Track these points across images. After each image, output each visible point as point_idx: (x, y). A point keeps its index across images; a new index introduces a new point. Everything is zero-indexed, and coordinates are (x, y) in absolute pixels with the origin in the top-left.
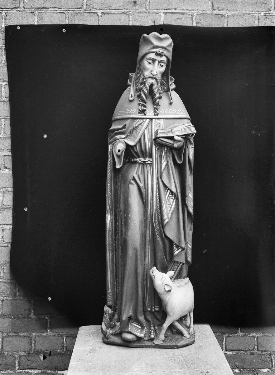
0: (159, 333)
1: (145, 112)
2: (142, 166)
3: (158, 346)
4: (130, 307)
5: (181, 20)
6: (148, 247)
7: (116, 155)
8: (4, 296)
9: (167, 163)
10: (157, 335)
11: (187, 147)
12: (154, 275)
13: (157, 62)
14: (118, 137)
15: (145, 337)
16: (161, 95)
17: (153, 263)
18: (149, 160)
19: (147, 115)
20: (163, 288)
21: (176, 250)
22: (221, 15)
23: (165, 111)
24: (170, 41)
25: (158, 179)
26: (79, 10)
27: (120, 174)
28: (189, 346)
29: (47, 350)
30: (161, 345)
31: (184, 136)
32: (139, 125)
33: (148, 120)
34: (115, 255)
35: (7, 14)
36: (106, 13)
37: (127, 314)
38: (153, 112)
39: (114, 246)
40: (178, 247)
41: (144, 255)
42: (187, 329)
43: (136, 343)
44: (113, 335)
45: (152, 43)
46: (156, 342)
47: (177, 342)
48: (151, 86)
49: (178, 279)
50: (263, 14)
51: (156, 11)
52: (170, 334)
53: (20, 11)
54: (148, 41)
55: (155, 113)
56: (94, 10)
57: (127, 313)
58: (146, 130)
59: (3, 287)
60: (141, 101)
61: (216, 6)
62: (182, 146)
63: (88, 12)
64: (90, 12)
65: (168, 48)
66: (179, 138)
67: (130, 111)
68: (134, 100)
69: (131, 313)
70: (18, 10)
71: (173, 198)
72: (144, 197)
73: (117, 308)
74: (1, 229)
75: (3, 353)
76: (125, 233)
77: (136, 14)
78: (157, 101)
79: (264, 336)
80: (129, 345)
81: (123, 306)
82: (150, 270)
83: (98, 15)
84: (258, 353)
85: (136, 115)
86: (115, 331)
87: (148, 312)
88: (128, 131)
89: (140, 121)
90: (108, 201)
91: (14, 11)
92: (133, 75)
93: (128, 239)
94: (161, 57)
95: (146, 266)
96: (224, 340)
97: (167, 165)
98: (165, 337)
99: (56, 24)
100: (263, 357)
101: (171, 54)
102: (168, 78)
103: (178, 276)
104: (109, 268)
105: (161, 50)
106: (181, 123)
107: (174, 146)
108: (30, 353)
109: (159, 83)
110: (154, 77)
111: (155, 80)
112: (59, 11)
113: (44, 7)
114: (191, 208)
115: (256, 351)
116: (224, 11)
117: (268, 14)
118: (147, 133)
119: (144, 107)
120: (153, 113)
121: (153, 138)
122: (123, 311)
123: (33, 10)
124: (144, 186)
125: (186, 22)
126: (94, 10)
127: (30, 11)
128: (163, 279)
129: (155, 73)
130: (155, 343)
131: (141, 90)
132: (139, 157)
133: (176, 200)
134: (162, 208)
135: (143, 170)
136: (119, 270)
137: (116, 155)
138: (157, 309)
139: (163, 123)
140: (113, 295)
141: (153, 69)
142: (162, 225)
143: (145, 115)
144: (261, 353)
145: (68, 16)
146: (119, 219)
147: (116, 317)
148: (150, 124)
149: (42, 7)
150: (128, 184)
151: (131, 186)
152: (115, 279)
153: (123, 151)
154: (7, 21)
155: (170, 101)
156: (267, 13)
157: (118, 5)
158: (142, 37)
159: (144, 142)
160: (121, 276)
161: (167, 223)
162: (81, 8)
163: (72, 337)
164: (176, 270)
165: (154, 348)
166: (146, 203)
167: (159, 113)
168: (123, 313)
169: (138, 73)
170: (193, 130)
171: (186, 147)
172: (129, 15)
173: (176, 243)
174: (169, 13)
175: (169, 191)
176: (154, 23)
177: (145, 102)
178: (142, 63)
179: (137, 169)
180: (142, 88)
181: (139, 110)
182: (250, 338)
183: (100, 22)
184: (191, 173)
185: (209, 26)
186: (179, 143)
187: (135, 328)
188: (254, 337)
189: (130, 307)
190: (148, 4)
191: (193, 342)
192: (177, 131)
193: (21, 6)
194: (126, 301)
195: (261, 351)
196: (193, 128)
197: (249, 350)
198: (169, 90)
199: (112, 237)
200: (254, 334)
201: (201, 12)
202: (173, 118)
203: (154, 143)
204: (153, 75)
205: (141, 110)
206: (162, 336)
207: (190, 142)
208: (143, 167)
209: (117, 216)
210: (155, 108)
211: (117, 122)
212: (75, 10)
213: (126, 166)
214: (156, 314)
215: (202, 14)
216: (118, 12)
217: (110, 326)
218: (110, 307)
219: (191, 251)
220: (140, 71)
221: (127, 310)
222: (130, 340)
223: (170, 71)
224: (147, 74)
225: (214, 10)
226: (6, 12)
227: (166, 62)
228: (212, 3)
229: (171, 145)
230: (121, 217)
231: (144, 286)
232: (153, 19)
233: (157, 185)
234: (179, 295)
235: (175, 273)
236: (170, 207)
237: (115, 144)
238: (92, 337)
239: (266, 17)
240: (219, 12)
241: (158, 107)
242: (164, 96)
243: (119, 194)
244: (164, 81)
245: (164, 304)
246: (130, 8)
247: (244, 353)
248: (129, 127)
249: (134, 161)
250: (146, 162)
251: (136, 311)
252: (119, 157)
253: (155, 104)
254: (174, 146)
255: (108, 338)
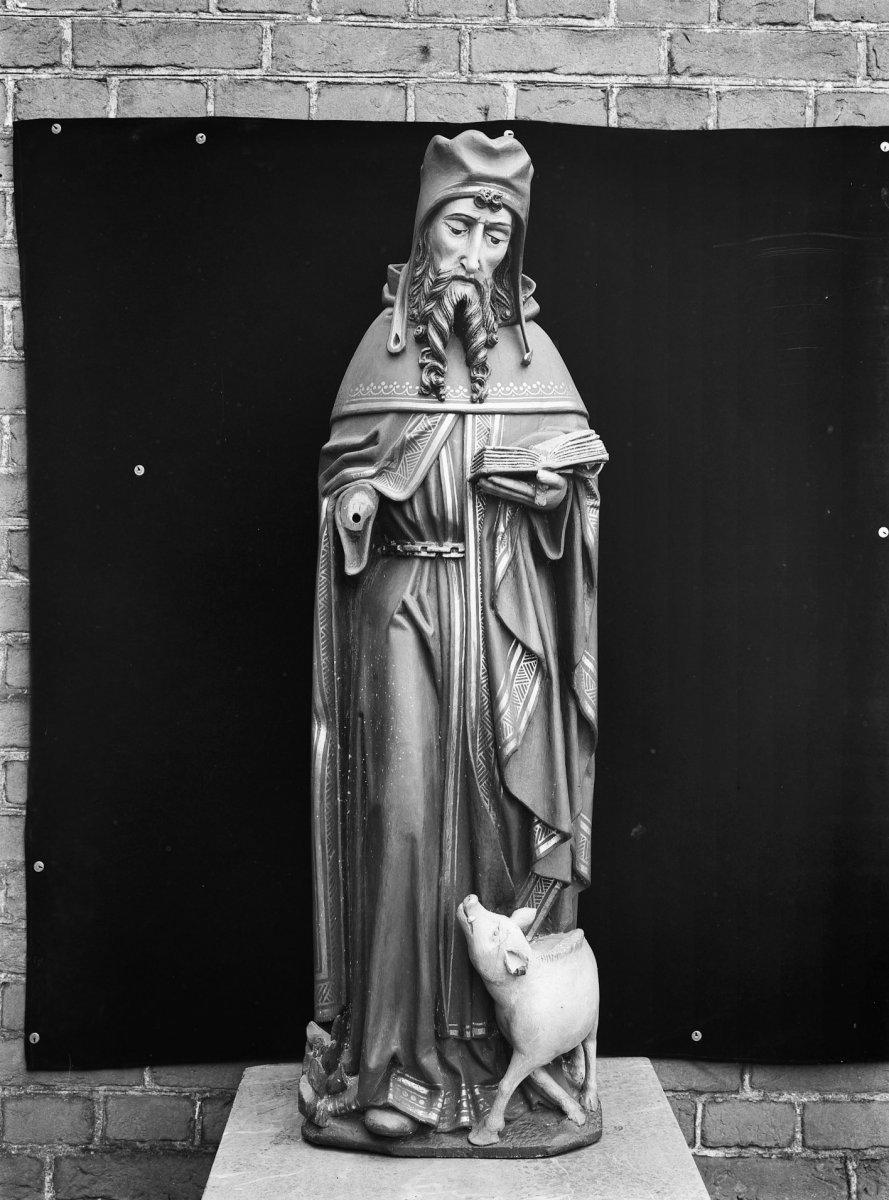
0: (485, 1107)
1: (441, 393)
2: (430, 569)
3: (483, 1150)
4: (391, 1027)
5: (570, 107)
6: (451, 831)
7: (347, 530)
8: (9, 972)
9: (514, 557)
10: (479, 1116)
11: (579, 504)
12: (471, 923)
13: (480, 228)
14: (351, 471)
15: (440, 1121)
16: (495, 337)
17: (467, 884)
18: (455, 549)
19: (449, 402)
20: (500, 965)
21: (543, 839)
22: (699, 89)
23: (506, 389)
24: (524, 158)
25: (484, 611)
26: (247, 72)
27: (359, 596)
28: (585, 1152)
29: (142, 1142)
30: (494, 1146)
31: (570, 471)
32: (423, 433)
33: (451, 417)
34: (344, 858)
35: (21, 86)
36: (334, 83)
37: (383, 1050)
38: (466, 390)
39: (339, 828)
40: (549, 829)
41: (437, 856)
42: (575, 1095)
43: (414, 1143)
44: (336, 1115)
45: (463, 167)
46: (478, 1139)
47: (543, 1138)
48: (462, 305)
49: (548, 933)
50: (831, 90)
51: (491, 77)
52: (521, 1111)
53: (62, 76)
54: (450, 160)
55: (475, 396)
56: (292, 73)
57: (383, 1043)
58: (444, 450)
59: (5, 943)
60: (428, 357)
61: (681, 62)
62: (558, 508)
63: (276, 78)
64: (283, 78)
65: (516, 183)
66: (554, 478)
67: (391, 386)
68: (403, 350)
69: (395, 1046)
70: (56, 71)
71: (533, 673)
72: (438, 669)
73: (351, 1028)
74: (2, 761)
75: (5, 1150)
76: (377, 786)
77: (429, 88)
78: (481, 355)
79: (826, 1101)
80: (390, 1148)
81: (371, 1022)
82: (457, 906)
83: (308, 90)
84: (804, 1155)
85: (412, 401)
86: (342, 1105)
87: (449, 1042)
88: (387, 455)
89: (426, 422)
90: (320, 682)
91: (44, 74)
92: (400, 269)
93: (386, 806)
94: (493, 211)
95: (443, 891)
96: (699, 1115)
97: (514, 563)
98: (507, 1121)
99: (174, 115)
100: (820, 1166)
101: (527, 201)
102: (517, 283)
103: (549, 925)
104: (321, 899)
105: (494, 190)
106: (559, 428)
107: (537, 502)
108: (89, 1150)
109: (488, 295)
110: (472, 276)
111: (473, 286)
112: (184, 78)
113: (139, 62)
114: (590, 703)
115: (797, 1149)
116: (706, 80)
117: (846, 90)
118: (448, 461)
119: (437, 374)
120: (466, 394)
121: (469, 475)
122: (368, 1041)
123: (103, 72)
124: (437, 632)
125: (585, 112)
126: (292, 73)
127: (95, 77)
128: (502, 935)
129: (473, 264)
130: (473, 1141)
131: (426, 319)
132: (422, 539)
133: (542, 679)
134: (497, 703)
135: (434, 581)
136: (354, 906)
137: (347, 530)
138: (480, 1032)
139: (500, 427)
140: (337, 988)
141: (468, 249)
142: (498, 761)
143: (442, 401)
144: (814, 1156)
145: (215, 91)
146: (354, 739)
147: (345, 1059)
148: (458, 432)
149: (132, 62)
150: (384, 628)
151: (394, 633)
152: (343, 936)
153: (369, 519)
154: (19, 109)
155: (522, 354)
156: (845, 84)
157: (371, 58)
158: (431, 145)
159: (437, 488)
160: (363, 925)
161: (515, 751)
162: (255, 68)
163: (220, 1099)
164: (542, 905)
165: (470, 1156)
166: (445, 691)
167: (486, 396)
168: (368, 1045)
169: (417, 265)
170: (596, 450)
171: (575, 504)
172: (405, 88)
173: (542, 816)
174: (533, 83)
175: (519, 650)
176: (486, 114)
177: (441, 360)
178: (431, 230)
179: (416, 578)
180: (432, 314)
181: (422, 384)
182: (779, 1108)
183: (313, 111)
184: (590, 591)
185: (658, 127)
186: (553, 494)
187: (410, 1095)
188: (791, 1104)
189: (391, 1027)
190: (465, 54)
191: (596, 1138)
192: (546, 454)
193: (67, 60)
194: (380, 1007)
195: (816, 1150)
196: (599, 445)
197: (777, 1146)
198: (518, 321)
199: (332, 799)
200: (794, 1097)
201: (634, 80)
202: (534, 410)
203: (470, 493)
204: (468, 272)
205: (427, 384)
206: (496, 1120)
207: (589, 490)
208: (433, 570)
209: (347, 730)
210: (473, 380)
211: (347, 424)
212: (237, 72)
213: (378, 568)
214: (476, 1046)
215: (637, 86)
216: (371, 81)
217: (326, 1089)
218: (326, 1025)
219: (589, 842)
220: (423, 258)
221: (381, 1035)
222: (394, 1132)
223: (521, 259)
224: (447, 266)
225: (677, 74)
226: (19, 77)
227: (509, 229)
228: (670, 53)
229: (526, 498)
230: (363, 733)
231: (439, 959)
232: (483, 105)
233: (481, 631)
234: (554, 986)
235: (538, 913)
236: (523, 700)
237: (342, 495)
238: (282, 1100)
239: (840, 97)
240: (690, 80)
241: (485, 376)
242: (502, 337)
243: (354, 658)
244: (504, 289)
245: (502, 1015)
246: (407, 68)
247: (761, 1156)
248: (389, 440)
249: (406, 551)
250: (444, 555)
251: (411, 1041)
252: (356, 537)
253: (473, 363)
254: (537, 502)
255: (319, 1128)
